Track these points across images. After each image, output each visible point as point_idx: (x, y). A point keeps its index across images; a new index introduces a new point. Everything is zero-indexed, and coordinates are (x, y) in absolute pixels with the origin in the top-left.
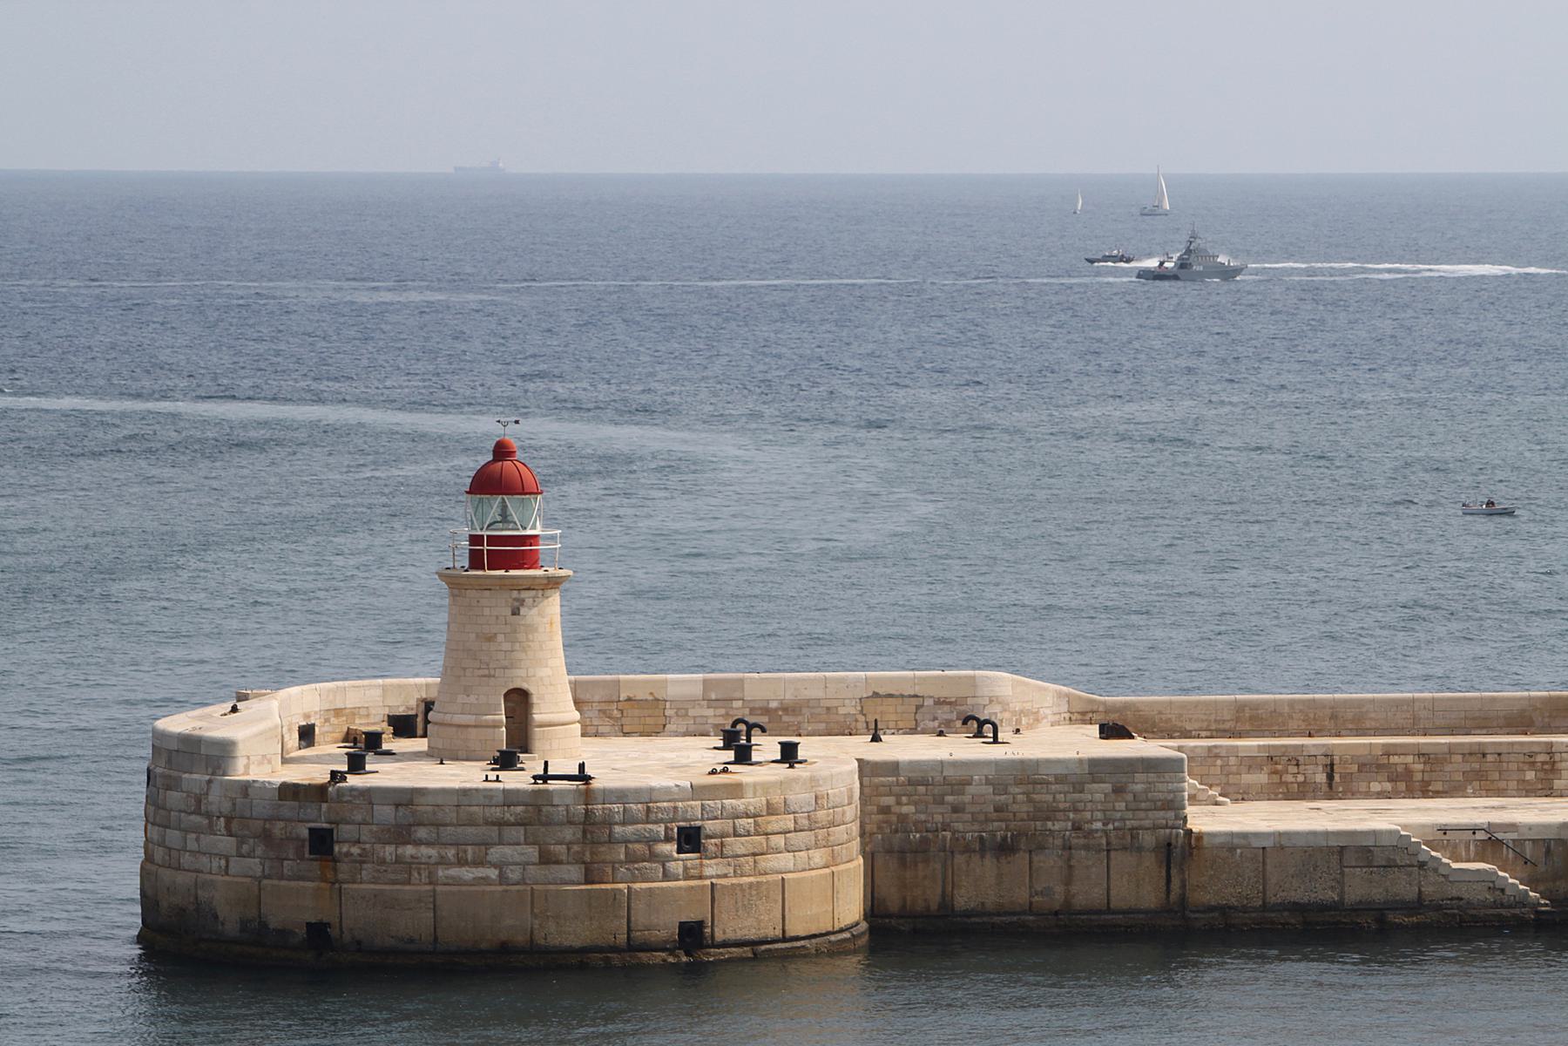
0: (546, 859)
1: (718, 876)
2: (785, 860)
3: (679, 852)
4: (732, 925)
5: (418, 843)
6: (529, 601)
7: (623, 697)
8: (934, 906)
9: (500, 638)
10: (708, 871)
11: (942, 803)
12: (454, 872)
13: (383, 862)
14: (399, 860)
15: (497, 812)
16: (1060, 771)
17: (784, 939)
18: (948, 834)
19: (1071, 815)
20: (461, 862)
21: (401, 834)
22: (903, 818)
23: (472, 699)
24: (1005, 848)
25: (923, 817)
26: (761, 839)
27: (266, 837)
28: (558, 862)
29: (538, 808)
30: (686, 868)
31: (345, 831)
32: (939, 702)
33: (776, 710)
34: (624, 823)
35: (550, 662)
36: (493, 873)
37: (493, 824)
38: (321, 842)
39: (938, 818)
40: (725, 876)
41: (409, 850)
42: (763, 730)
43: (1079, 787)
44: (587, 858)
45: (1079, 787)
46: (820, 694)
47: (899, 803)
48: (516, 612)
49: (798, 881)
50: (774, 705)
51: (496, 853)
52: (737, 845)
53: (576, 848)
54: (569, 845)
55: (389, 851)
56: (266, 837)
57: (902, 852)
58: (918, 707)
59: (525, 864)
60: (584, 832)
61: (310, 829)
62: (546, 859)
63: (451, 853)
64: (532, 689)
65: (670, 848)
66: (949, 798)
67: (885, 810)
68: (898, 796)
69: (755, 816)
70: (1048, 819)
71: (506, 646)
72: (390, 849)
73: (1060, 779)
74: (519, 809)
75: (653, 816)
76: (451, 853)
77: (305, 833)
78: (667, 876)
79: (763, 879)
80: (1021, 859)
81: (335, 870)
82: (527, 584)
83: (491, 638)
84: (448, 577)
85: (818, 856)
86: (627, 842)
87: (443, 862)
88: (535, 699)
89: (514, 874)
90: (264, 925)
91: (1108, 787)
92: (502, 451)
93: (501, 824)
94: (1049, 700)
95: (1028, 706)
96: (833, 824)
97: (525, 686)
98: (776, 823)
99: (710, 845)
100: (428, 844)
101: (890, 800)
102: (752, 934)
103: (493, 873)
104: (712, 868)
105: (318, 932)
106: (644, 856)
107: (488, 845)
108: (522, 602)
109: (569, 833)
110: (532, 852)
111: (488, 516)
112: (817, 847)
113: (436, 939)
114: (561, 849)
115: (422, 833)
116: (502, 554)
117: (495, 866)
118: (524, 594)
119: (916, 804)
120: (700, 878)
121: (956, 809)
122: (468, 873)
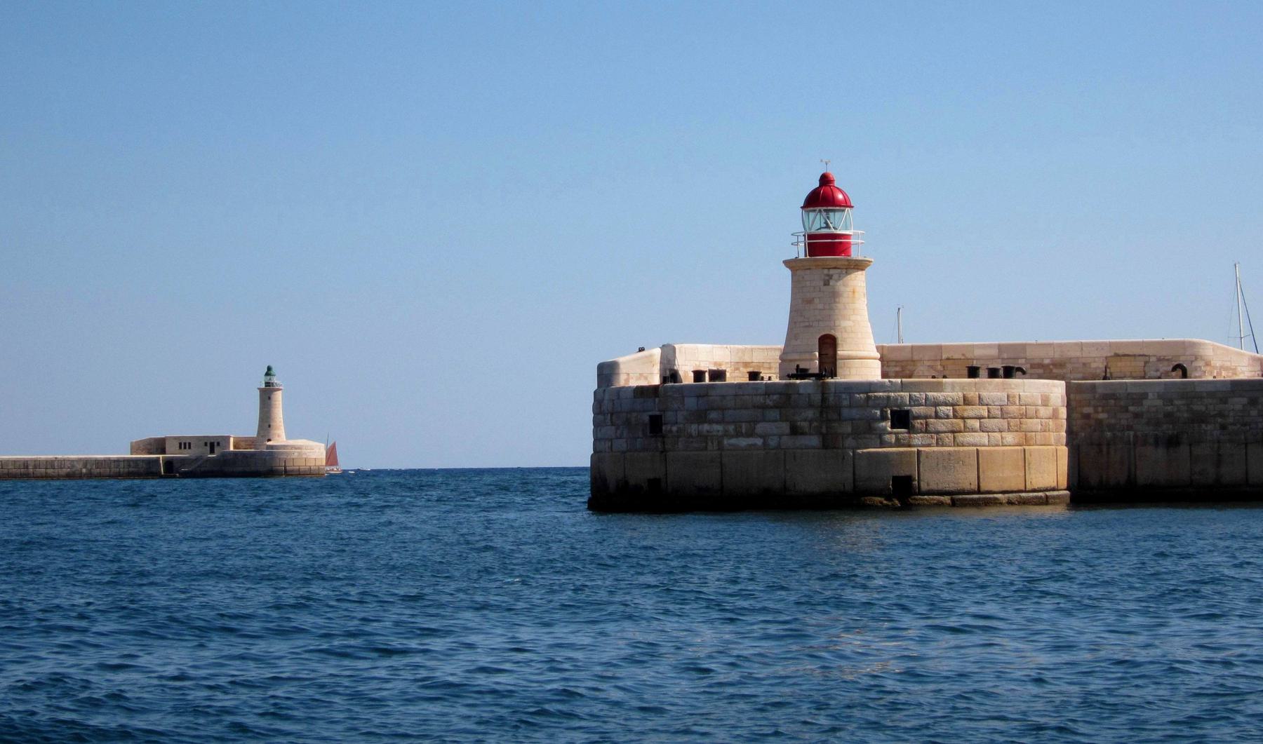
0: (795, 431)
1: (923, 446)
2: (982, 438)
3: (892, 427)
4: (930, 479)
5: (711, 422)
6: (835, 277)
7: (944, 357)
8: (772, 376)
9: (817, 301)
10: (916, 442)
11: (1127, 411)
12: (733, 441)
13: (691, 436)
14: (700, 435)
15: (760, 399)
16: (1210, 389)
17: (979, 492)
18: (1132, 433)
19: (1220, 420)
20: (738, 434)
21: (700, 416)
22: (1099, 422)
23: (799, 342)
24: (1172, 442)
25: (1113, 421)
26: (960, 422)
27: (628, 423)
28: (803, 434)
29: (788, 396)
30: (897, 439)
31: (669, 416)
32: (1160, 360)
33: (1048, 365)
34: (850, 406)
35: (853, 318)
36: (759, 442)
37: (758, 407)
38: (656, 424)
39: (1124, 422)
40: (929, 445)
41: (706, 427)
42: (1024, 373)
43: (1224, 401)
44: (824, 430)
45: (1224, 401)
46: (1078, 354)
47: (1097, 412)
48: (826, 283)
49: (990, 453)
50: (1047, 362)
51: (760, 428)
52: (940, 425)
53: (815, 424)
54: (811, 422)
55: (693, 429)
56: (628, 423)
57: (1099, 445)
58: (1146, 363)
59: (780, 436)
60: (821, 413)
61: (651, 417)
62: (795, 431)
63: (731, 428)
64: (838, 335)
65: (887, 425)
66: (1131, 408)
67: (1087, 416)
68: (1095, 407)
69: (952, 405)
70: (1203, 422)
71: (820, 306)
72: (694, 427)
73: (1212, 395)
74: (775, 397)
75: (871, 403)
76: (731, 428)
77: (647, 419)
78: (883, 444)
79: (961, 449)
80: (1184, 449)
81: (664, 443)
82: (834, 264)
83: (810, 301)
84: (791, 264)
85: (1010, 438)
86: (852, 420)
87: (726, 434)
88: (839, 341)
89: (773, 442)
90: (627, 482)
91: (1245, 400)
92: (825, 180)
93: (764, 407)
94: (1245, 362)
95: (1228, 364)
96: (1025, 416)
97: (832, 333)
98: (970, 411)
99: (918, 423)
100: (718, 422)
101: (1087, 410)
102: (951, 487)
103: (759, 442)
104: (918, 439)
105: (654, 483)
106: (867, 431)
107: (756, 422)
108: (830, 277)
109: (810, 414)
110: (785, 427)
111: (816, 222)
112: (1009, 430)
113: (1247, 473)
114: (805, 424)
115: (713, 415)
116: (826, 248)
117: (761, 436)
118: (832, 272)
119: (1108, 412)
120: (910, 446)
121: (1137, 416)
122: (743, 442)
